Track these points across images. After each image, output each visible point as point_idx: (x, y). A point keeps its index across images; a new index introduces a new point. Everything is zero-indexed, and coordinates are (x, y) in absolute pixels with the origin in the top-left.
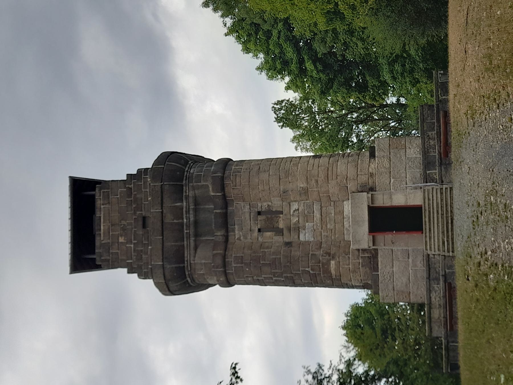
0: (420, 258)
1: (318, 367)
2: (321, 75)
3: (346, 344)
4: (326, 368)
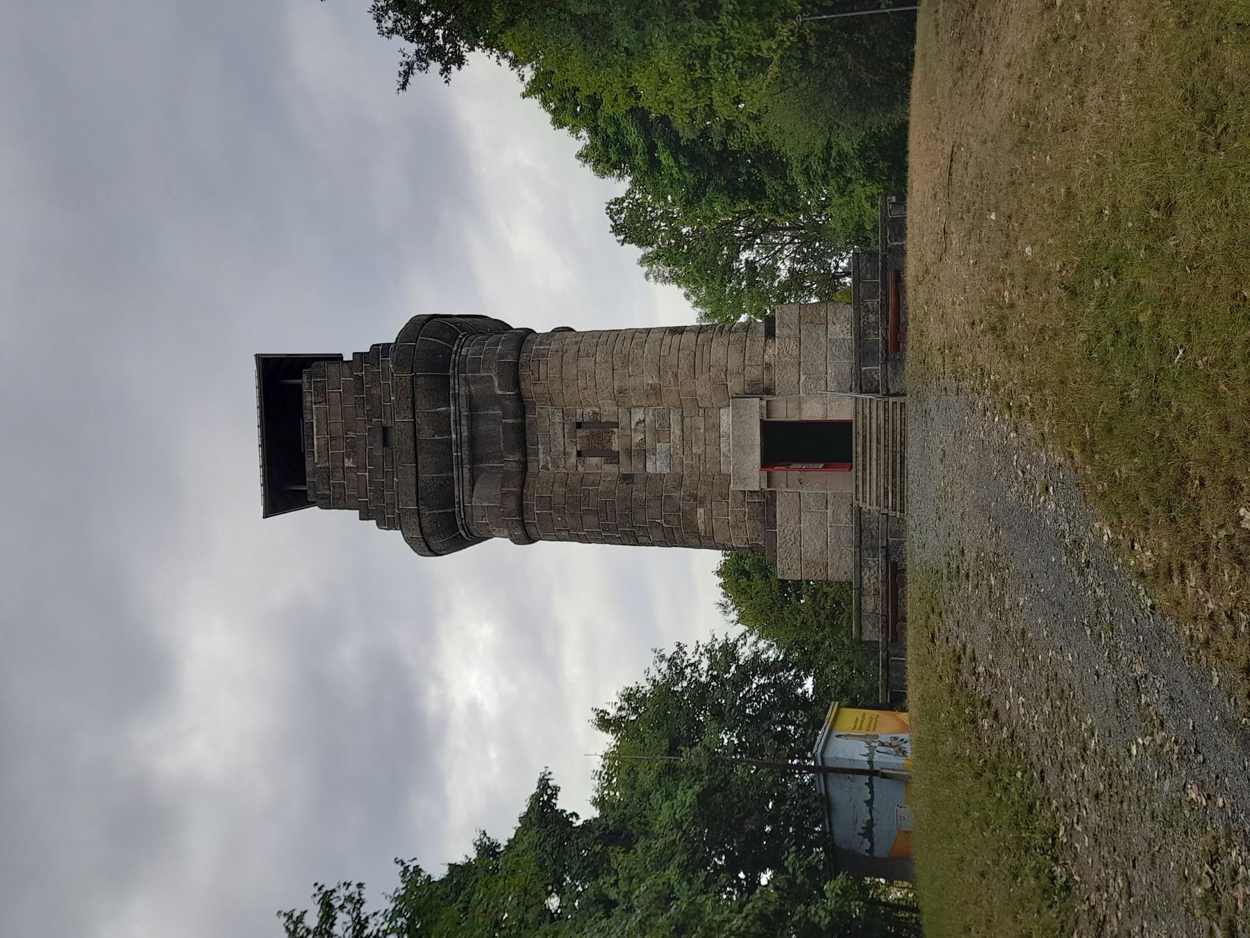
0: (847, 508)
1: (676, 649)
2: (686, 173)
3: (724, 600)
4: (690, 650)
